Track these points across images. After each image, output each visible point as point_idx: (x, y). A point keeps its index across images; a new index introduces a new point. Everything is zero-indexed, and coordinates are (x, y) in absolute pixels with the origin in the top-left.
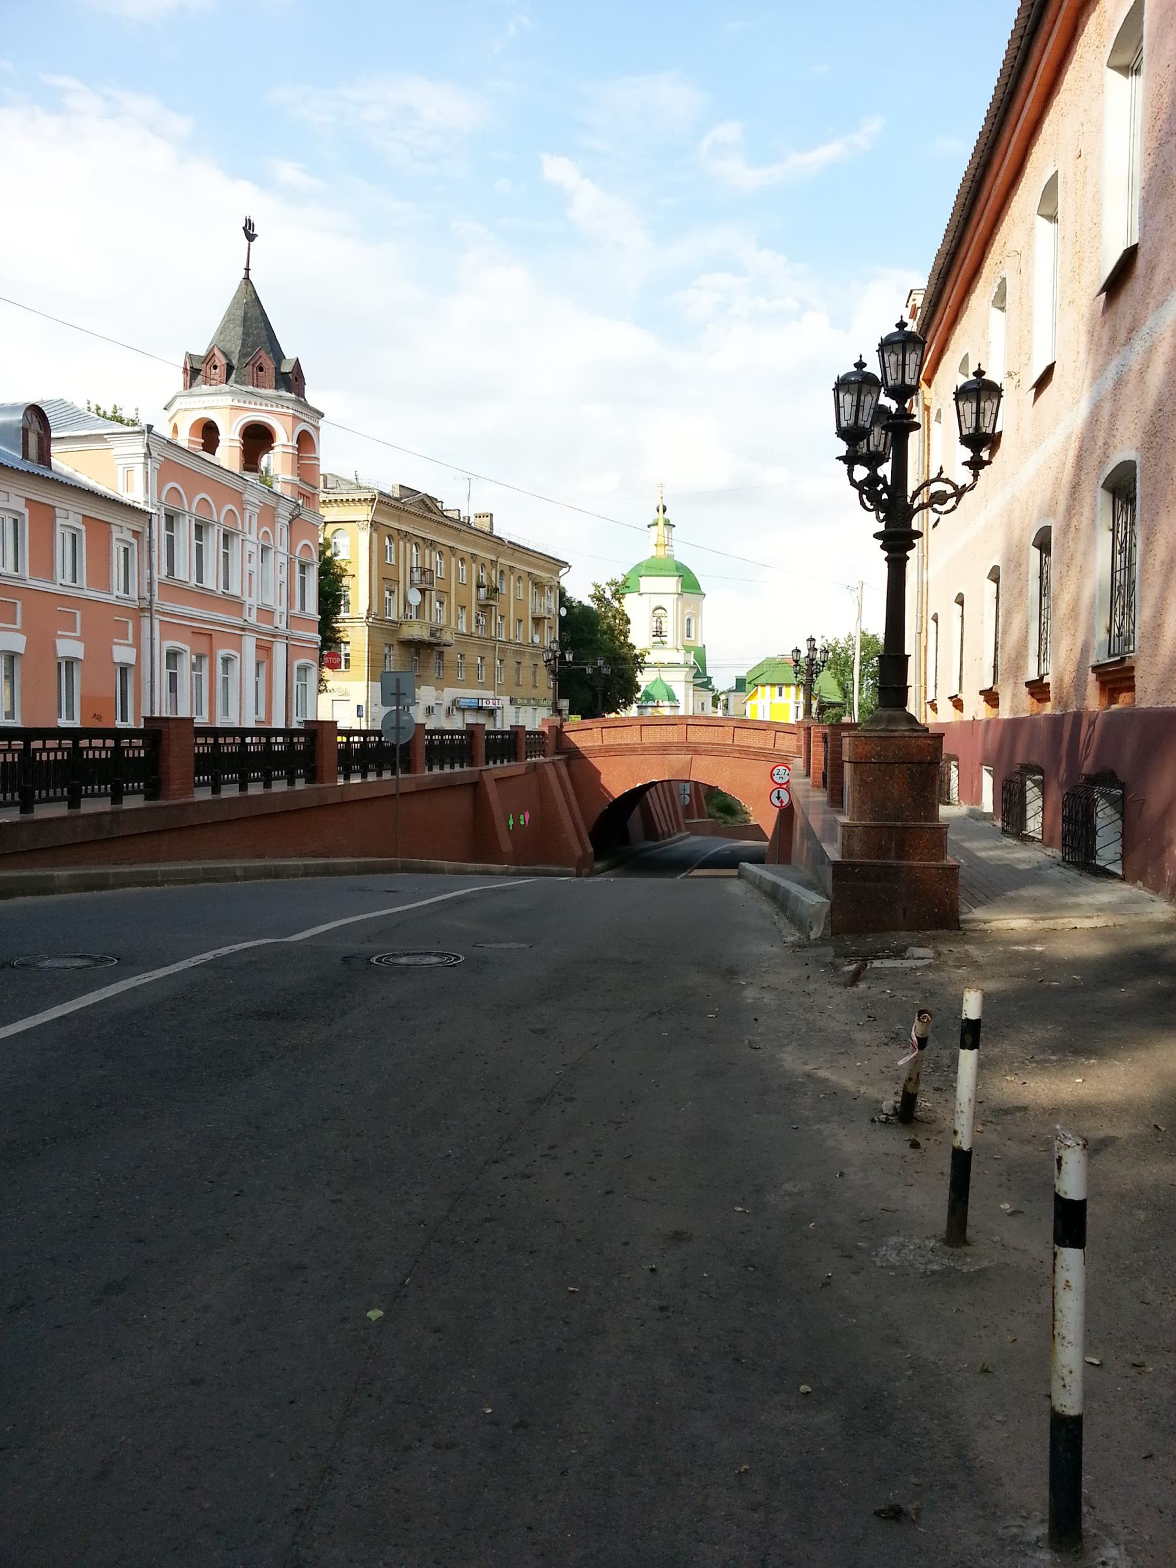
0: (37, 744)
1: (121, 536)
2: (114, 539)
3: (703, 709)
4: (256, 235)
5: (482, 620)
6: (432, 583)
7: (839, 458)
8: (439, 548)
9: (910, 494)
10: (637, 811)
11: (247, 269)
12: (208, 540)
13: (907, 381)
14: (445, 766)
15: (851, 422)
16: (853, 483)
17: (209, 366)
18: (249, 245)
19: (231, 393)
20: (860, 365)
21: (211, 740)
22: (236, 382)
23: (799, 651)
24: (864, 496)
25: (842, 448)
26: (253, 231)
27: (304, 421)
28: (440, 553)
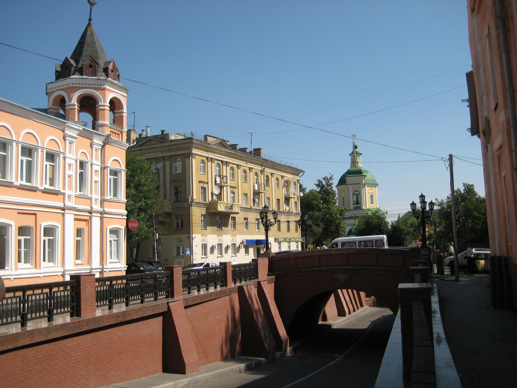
0: (55, 289)
3: (43, 267)
8: (231, 165)
11: (90, 20)
14: (210, 288)
27: (115, 92)
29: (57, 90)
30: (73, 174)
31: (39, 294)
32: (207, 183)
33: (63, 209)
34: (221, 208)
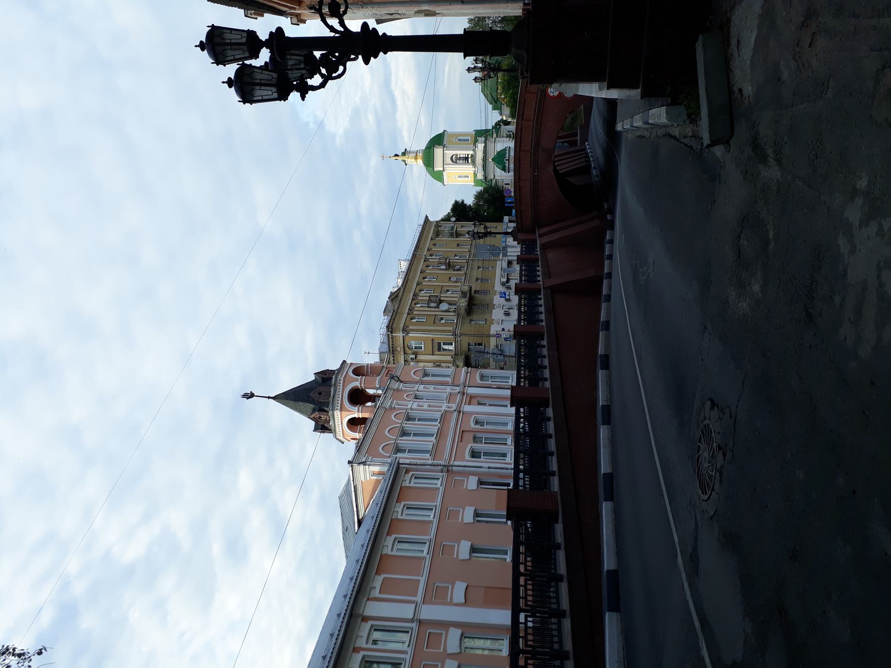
0: (522, 568)
1: (390, 547)
2: (410, 485)
4: (251, 392)
5: (457, 267)
6: (437, 296)
7: (303, 99)
9: (332, 34)
10: (571, 179)
11: (269, 398)
12: (411, 430)
13: (244, 40)
14: (540, 318)
15: (274, 89)
16: (323, 85)
17: (319, 421)
18: (256, 396)
19: (333, 410)
20: (230, 83)
21: (522, 380)
22: (328, 407)
23: (476, 78)
24: (334, 75)
25: (295, 96)
26: (248, 394)
27: (347, 372)
28: (420, 291)
29: (342, 427)
30: (427, 404)
31: (526, 590)
32: (442, 287)
33: (460, 412)
34: (463, 303)
